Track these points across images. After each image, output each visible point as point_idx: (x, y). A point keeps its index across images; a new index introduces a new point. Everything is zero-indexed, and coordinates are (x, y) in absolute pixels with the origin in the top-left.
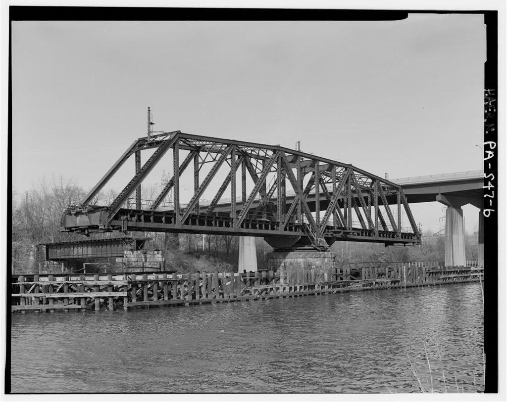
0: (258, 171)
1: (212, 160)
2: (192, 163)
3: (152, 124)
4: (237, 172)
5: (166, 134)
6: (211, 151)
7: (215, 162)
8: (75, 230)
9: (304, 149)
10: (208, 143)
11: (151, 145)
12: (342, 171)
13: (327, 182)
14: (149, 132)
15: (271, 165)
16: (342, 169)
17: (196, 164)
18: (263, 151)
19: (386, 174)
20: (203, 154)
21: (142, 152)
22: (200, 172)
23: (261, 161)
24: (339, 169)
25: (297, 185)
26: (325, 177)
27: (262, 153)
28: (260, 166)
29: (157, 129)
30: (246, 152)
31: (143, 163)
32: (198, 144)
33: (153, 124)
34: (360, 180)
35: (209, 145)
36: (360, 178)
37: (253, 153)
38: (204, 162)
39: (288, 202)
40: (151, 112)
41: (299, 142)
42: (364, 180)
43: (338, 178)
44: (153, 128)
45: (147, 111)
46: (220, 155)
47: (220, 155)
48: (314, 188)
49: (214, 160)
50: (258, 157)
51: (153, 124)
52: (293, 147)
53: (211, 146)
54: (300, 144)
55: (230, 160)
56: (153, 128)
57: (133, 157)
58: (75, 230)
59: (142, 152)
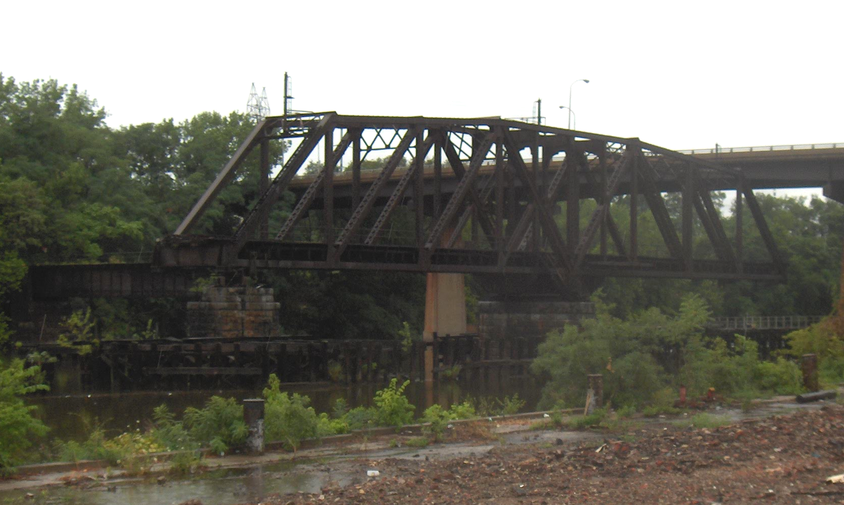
1: (384, 146)
3: (290, 98)
33: (292, 98)
40: (289, 79)
41: (539, 102)
51: (292, 98)
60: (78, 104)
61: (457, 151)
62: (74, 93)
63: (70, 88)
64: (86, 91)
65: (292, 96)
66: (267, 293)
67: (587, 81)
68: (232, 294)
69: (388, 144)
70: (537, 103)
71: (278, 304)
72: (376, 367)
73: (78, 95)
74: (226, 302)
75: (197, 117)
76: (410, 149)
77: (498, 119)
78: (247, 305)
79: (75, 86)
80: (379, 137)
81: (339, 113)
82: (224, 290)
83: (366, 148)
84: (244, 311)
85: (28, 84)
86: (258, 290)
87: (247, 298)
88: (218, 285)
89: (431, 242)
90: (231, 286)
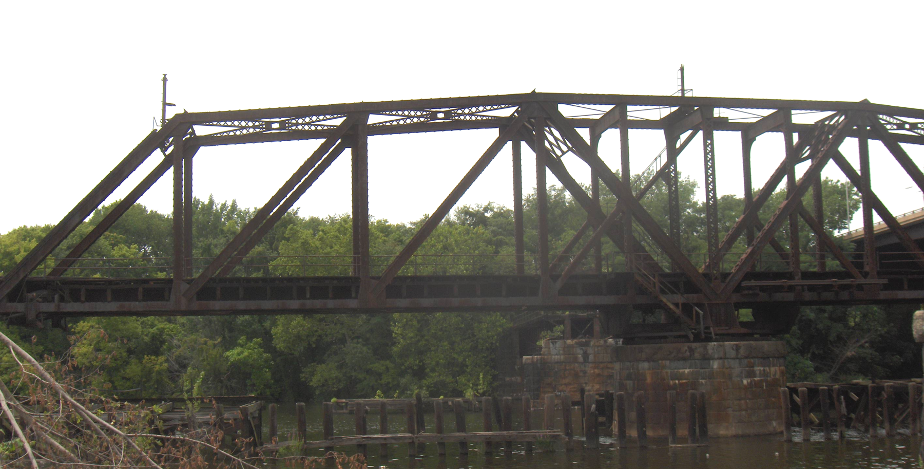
41: (682, 69)
64: (689, 176)
78: (591, 358)
82: (559, 343)
87: (590, 351)
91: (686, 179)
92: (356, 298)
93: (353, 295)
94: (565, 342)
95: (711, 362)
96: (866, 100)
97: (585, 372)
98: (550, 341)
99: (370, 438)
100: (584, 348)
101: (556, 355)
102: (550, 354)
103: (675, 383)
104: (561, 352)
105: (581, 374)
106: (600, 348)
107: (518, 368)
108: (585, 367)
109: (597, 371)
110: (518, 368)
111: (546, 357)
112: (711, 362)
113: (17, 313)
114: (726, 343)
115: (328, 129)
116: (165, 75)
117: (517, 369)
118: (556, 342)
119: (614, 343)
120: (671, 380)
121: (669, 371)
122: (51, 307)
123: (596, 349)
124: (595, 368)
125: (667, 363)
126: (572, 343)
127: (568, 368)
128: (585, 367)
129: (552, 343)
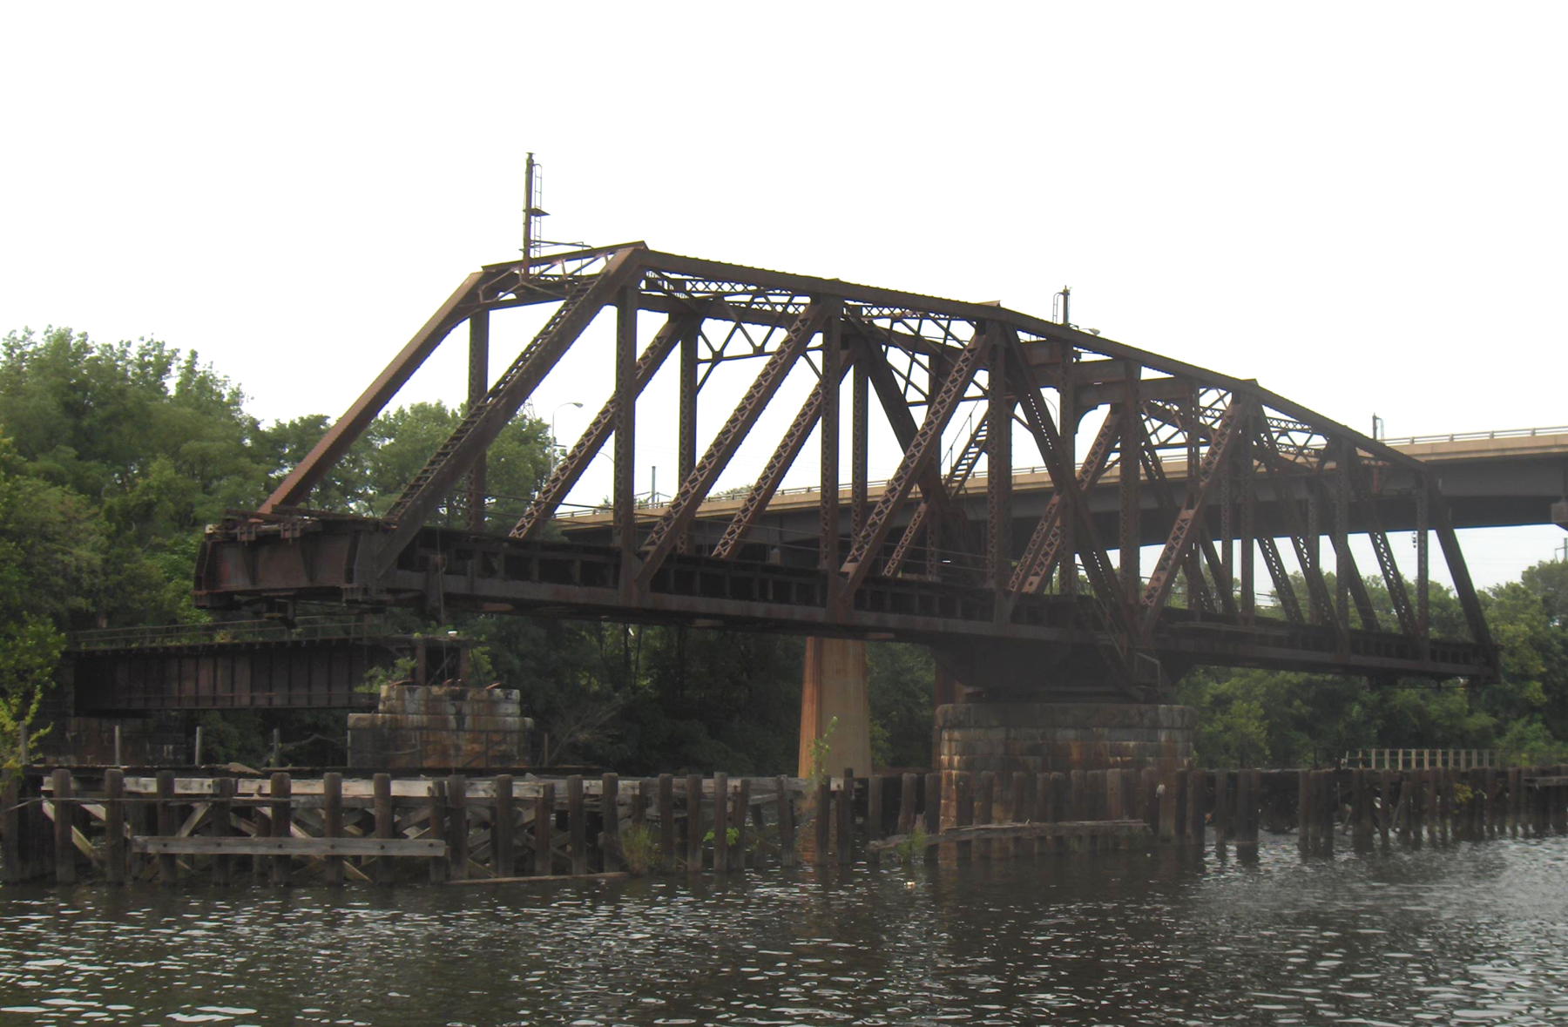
0: (912, 395)
1: (750, 351)
2: (674, 360)
3: (539, 213)
4: (842, 387)
5: (593, 253)
6: (742, 316)
7: (767, 359)
8: (248, 604)
9: (1082, 321)
10: (739, 288)
11: (533, 293)
12: (1220, 406)
13: (1164, 445)
14: (528, 243)
15: (969, 379)
16: (1221, 398)
17: (690, 363)
18: (934, 320)
19: (1375, 418)
20: (714, 330)
21: (495, 316)
22: (699, 397)
23: (924, 359)
24: (1208, 398)
25: (1056, 447)
26: (1157, 423)
27: (931, 330)
28: (921, 378)
29: (555, 233)
30: (871, 322)
31: (498, 368)
32: (701, 288)
33: (545, 214)
34: (1284, 440)
35: (739, 296)
36: (1284, 432)
37: (899, 327)
38: (718, 358)
39: (1019, 512)
40: (536, 170)
41: (1066, 294)
42: (1300, 438)
43: (1206, 431)
44: (541, 228)
45: (524, 167)
46: (780, 335)
47: (780, 335)
48: (1115, 462)
49: (759, 351)
50: (914, 344)
51: (545, 214)
52: (1045, 310)
53: (747, 298)
54: (1071, 298)
55: (820, 353)
56: (541, 228)
57: (461, 334)
58: (248, 604)
59: (495, 316)
60: (200, 389)
61: (901, 383)
62: (190, 369)
63: (184, 356)
64: (212, 363)
65: (543, 209)
66: (507, 698)
67: (579, 405)
68: (438, 699)
69: (758, 343)
70: (1062, 297)
71: (529, 720)
72: (736, 839)
73: (197, 368)
74: (427, 713)
75: (408, 410)
76: (809, 353)
77: (995, 305)
78: (468, 721)
79: (194, 354)
80: (738, 330)
81: (651, 247)
82: (420, 692)
83: (709, 355)
84: (461, 733)
85: (111, 347)
86: (490, 692)
87: (466, 709)
88: (412, 681)
89: (854, 560)
90: (439, 681)
91: (206, 369)
92: (823, 605)
93: (818, 600)
94: (429, 692)
95: (1159, 731)
96: (1255, 380)
97: (458, 748)
98: (406, 687)
99: (989, 829)
100: (456, 703)
101: (415, 713)
102: (404, 712)
103: (1117, 761)
104: (423, 709)
105: (452, 752)
106: (481, 705)
107: (72, 737)
108: (458, 738)
109: (477, 747)
110: (72, 737)
111: (399, 717)
112: (1159, 731)
113: (412, 590)
114: (1175, 706)
115: (545, 280)
116: (531, 155)
117: (70, 740)
118: (414, 690)
119: (504, 697)
120: (1112, 756)
121: (1108, 743)
122: (458, 585)
123: (476, 707)
124: (474, 741)
125: (1106, 731)
126: (440, 693)
127: (431, 739)
128: (458, 738)
129: (409, 690)
